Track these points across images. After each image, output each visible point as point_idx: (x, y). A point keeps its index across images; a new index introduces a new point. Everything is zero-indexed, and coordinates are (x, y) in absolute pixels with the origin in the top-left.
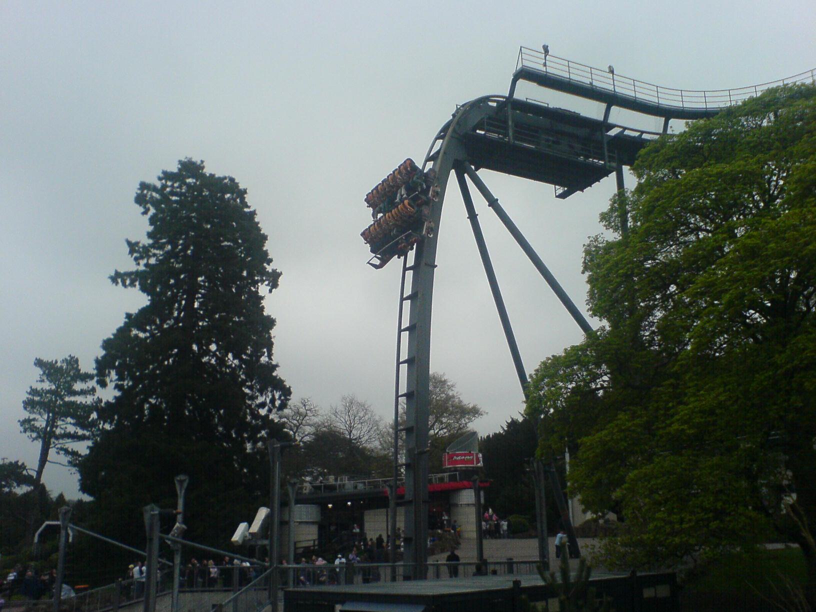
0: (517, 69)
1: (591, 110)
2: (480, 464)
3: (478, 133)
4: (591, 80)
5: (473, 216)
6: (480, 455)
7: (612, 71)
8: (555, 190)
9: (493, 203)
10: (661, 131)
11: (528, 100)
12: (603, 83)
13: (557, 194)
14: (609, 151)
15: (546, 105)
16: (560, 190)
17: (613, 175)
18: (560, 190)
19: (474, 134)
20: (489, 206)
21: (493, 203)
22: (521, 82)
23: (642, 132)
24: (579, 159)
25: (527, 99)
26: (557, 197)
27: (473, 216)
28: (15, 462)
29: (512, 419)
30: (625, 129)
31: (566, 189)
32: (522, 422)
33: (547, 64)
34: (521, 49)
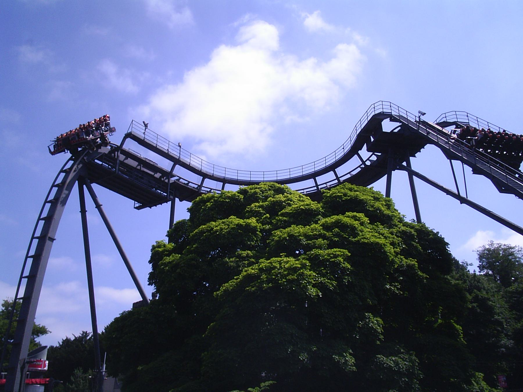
0: (128, 132)
1: (165, 164)
2: (46, 368)
3: (96, 162)
4: (168, 148)
5: (83, 211)
6: (47, 362)
7: (146, 126)
8: (135, 204)
9: (98, 206)
10: (200, 184)
11: (130, 150)
12: (175, 153)
13: (135, 207)
14: (170, 189)
15: (140, 155)
16: (137, 205)
17: (170, 203)
18: (137, 205)
19: (93, 161)
20: (96, 207)
21: (98, 206)
22: (128, 140)
23: (189, 182)
24: (112, 170)
25: (129, 149)
26: (134, 208)
27: (83, 211)
28: (110, 376)
29: (67, 338)
30: (180, 178)
31: (141, 205)
32: (74, 340)
33: (146, 134)
34: (132, 121)
